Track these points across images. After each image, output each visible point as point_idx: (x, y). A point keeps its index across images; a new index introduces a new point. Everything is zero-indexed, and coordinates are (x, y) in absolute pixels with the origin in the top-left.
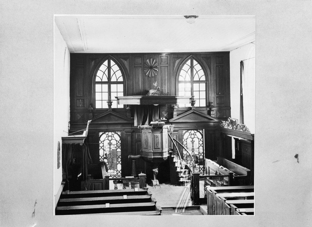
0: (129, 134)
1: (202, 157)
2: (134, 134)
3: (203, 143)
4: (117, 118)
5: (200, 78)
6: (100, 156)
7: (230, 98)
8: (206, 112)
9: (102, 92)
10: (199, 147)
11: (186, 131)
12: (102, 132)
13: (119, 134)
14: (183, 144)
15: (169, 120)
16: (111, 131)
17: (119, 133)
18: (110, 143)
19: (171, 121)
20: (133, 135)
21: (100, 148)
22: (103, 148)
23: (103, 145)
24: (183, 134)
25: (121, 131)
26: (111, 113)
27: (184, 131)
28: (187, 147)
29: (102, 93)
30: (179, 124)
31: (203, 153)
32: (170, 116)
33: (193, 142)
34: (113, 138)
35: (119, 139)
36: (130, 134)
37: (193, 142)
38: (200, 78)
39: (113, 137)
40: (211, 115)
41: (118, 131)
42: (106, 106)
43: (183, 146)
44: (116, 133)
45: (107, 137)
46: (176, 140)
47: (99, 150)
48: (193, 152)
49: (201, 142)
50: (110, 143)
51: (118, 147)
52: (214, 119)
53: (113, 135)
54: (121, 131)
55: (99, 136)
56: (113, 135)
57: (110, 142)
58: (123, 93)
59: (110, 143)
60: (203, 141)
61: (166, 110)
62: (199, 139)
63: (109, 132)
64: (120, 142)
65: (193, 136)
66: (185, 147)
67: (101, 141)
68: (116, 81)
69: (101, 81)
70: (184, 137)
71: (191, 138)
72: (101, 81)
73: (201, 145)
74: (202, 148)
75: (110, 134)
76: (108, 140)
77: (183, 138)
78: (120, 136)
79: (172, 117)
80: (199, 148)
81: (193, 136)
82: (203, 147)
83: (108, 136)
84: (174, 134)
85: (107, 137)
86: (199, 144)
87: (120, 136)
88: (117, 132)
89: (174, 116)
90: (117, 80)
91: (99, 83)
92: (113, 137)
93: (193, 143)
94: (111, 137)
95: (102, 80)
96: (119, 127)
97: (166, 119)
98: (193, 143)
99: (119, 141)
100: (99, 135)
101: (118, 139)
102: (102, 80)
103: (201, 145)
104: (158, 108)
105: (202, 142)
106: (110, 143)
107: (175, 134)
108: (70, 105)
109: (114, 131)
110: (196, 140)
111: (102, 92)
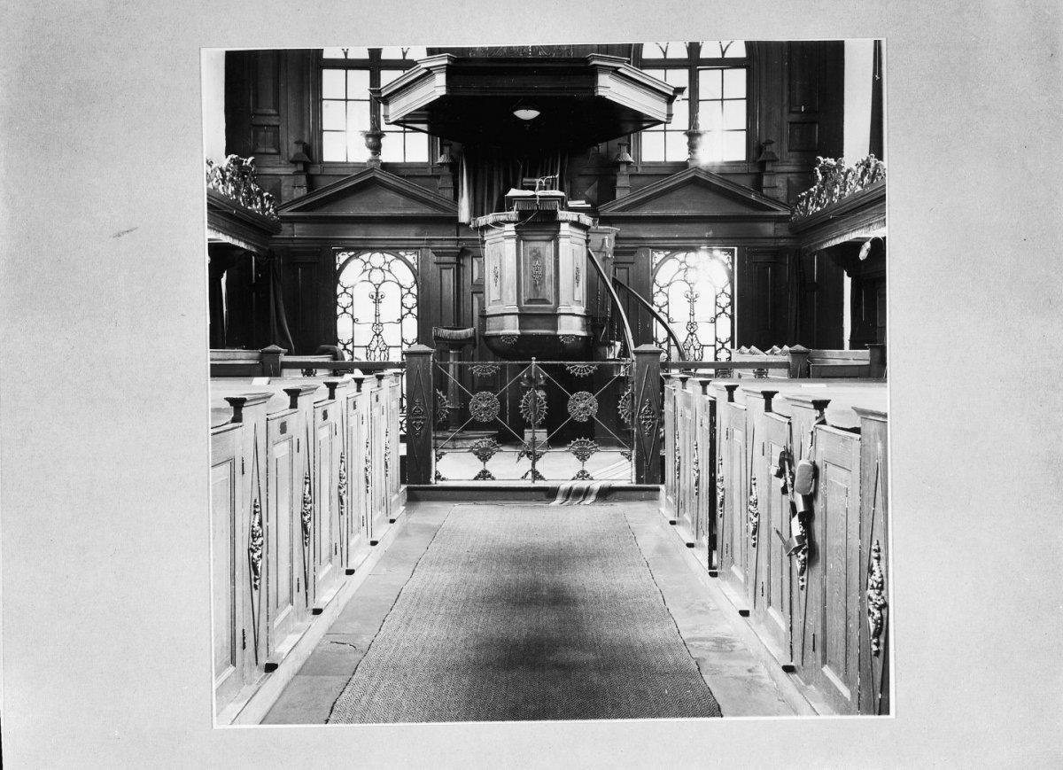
0: (446, 259)
1: (666, 356)
2: (467, 261)
3: (732, 304)
4: (402, 199)
5: (724, 49)
6: (339, 340)
7: (842, 129)
8: (745, 182)
9: (346, 100)
10: (715, 319)
11: (668, 253)
12: (347, 249)
13: (412, 261)
14: (653, 303)
15: (601, 208)
16: (382, 250)
17: (411, 258)
18: (377, 295)
19: (608, 210)
20: (463, 266)
21: (339, 310)
22: (719, 310)
23: (350, 300)
24: (654, 266)
25: (419, 248)
26: (370, 179)
27: (659, 256)
28: (668, 315)
29: (349, 102)
30: (667, 226)
31: (732, 339)
32: (606, 192)
33: (377, 299)
34: (389, 276)
35: (412, 279)
36: (452, 259)
37: (377, 299)
38: (724, 49)
39: (389, 271)
40: (764, 191)
41: (406, 249)
42: (362, 155)
43: (655, 309)
44: (399, 257)
45: (680, 270)
46: (626, 284)
47: (336, 317)
48: (692, 334)
49: (411, 301)
50: (377, 293)
51: (721, 310)
52: (296, 214)
53: (387, 265)
54: (419, 248)
55: (338, 267)
56: (389, 263)
57: (377, 289)
58: (744, 102)
59: (377, 295)
60: (732, 297)
61: (791, 169)
62: (401, 287)
63: (373, 250)
64: (414, 290)
65: (377, 276)
66: (661, 315)
67: (661, 285)
68: (401, 58)
69: (663, 57)
70: (657, 278)
71: (686, 282)
72: (663, 57)
73: (724, 311)
74: (729, 321)
75: (377, 259)
76: (685, 280)
77: (654, 281)
78: (416, 267)
79: (612, 196)
80: (715, 322)
81: (377, 276)
82: (732, 317)
83: (684, 266)
84: (621, 265)
85: (368, 272)
86: (716, 304)
87: (416, 267)
88: (402, 253)
89: (619, 194)
90: (723, 53)
91: (735, 63)
92: (387, 273)
93: (692, 301)
94: (382, 270)
95: (665, 54)
96: (410, 233)
97: (589, 206)
98: (692, 301)
99: (409, 287)
100: (335, 264)
101: (408, 278)
102: (665, 54)
103: (724, 311)
104: (557, 161)
105: (729, 300)
106: (377, 293)
107: (624, 265)
108: (225, 145)
109: (392, 249)
110: (391, 293)
111: (349, 98)
